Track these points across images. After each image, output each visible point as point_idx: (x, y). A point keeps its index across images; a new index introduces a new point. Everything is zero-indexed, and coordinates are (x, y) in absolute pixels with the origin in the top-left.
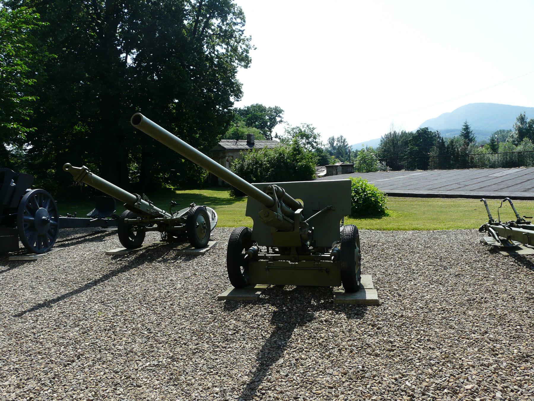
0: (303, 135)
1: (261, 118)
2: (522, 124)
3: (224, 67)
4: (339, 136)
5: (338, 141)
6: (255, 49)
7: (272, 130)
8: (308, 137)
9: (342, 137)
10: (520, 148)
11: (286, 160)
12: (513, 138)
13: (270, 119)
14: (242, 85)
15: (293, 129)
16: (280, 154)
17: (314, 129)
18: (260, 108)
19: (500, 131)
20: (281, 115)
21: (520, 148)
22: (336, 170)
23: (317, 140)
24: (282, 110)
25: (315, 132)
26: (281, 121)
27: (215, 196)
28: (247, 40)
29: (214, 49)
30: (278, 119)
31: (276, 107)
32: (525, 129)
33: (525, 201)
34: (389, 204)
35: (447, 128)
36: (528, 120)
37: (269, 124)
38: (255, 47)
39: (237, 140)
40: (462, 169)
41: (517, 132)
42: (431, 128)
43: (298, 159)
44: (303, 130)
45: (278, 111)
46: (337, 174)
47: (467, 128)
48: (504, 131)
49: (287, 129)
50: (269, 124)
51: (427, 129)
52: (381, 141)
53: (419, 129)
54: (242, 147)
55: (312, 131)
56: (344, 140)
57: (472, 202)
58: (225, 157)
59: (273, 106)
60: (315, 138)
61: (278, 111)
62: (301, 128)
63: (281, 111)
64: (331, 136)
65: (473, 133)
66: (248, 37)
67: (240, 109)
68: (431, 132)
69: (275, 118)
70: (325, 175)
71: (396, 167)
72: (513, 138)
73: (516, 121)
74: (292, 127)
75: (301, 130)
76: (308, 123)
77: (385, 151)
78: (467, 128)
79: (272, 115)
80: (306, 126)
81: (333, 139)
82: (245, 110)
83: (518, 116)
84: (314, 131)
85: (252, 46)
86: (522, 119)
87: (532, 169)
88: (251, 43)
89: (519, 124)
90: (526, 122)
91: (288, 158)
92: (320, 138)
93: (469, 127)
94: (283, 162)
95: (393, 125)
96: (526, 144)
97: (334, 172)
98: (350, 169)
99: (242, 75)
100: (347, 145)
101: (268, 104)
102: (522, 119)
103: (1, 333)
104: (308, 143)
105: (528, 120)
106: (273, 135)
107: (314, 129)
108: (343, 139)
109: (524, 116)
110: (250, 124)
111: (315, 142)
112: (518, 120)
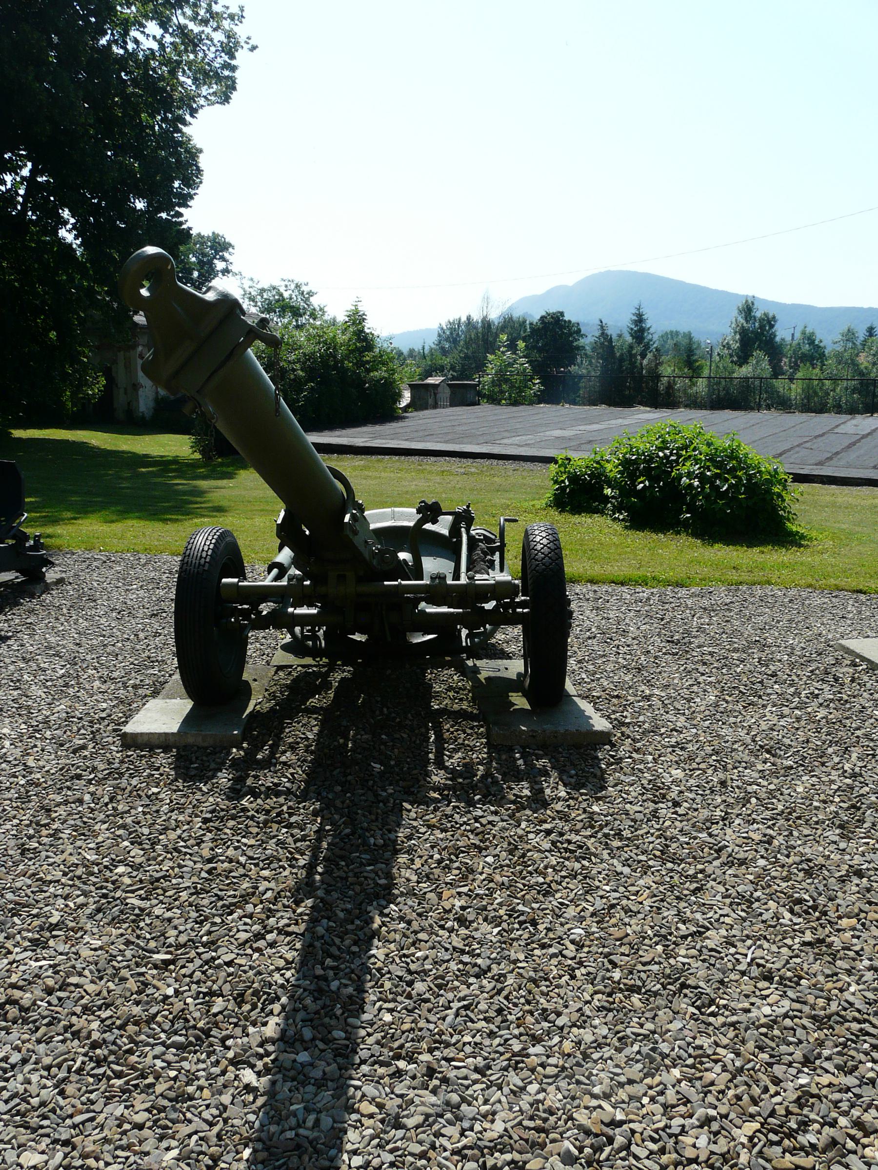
2: (747, 322)
6: (254, 48)
8: (296, 312)
10: (745, 371)
11: (342, 362)
12: (729, 348)
13: (201, 263)
14: (201, 151)
15: (263, 290)
17: (311, 294)
19: (672, 332)
20: (226, 255)
21: (745, 371)
22: (435, 394)
24: (230, 245)
25: (315, 301)
26: (226, 271)
27: (124, 448)
28: (232, 17)
29: (126, 33)
30: (220, 265)
31: (215, 236)
32: (752, 332)
34: (804, 507)
35: (597, 316)
37: (196, 274)
41: (738, 337)
42: (765, 302)
43: (368, 362)
44: (286, 295)
46: (435, 406)
47: (639, 319)
48: (677, 333)
49: (248, 290)
51: (562, 314)
52: (439, 335)
53: (544, 314)
55: (306, 301)
58: (134, 347)
62: (282, 289)
65: (651, 331)
66: (234, 10)
68: (570, 321)
69: (211, 263)
72: (729, 348)
73: (735, 313)
74: (260, 286)
75: (281, 295)
77: (467, 357)
78: (639, 319)
79: (204, 255)
80: (293, 286)
83: (740, 304)
84: (311, 299)
85: (242, 40)
88: (241, 31)
91: (346, 357)
93: (645, 317)
94: (335, 367)
95: (487, 300)
96: (757, 362)
97: (431, 401)
98: (470, 396)
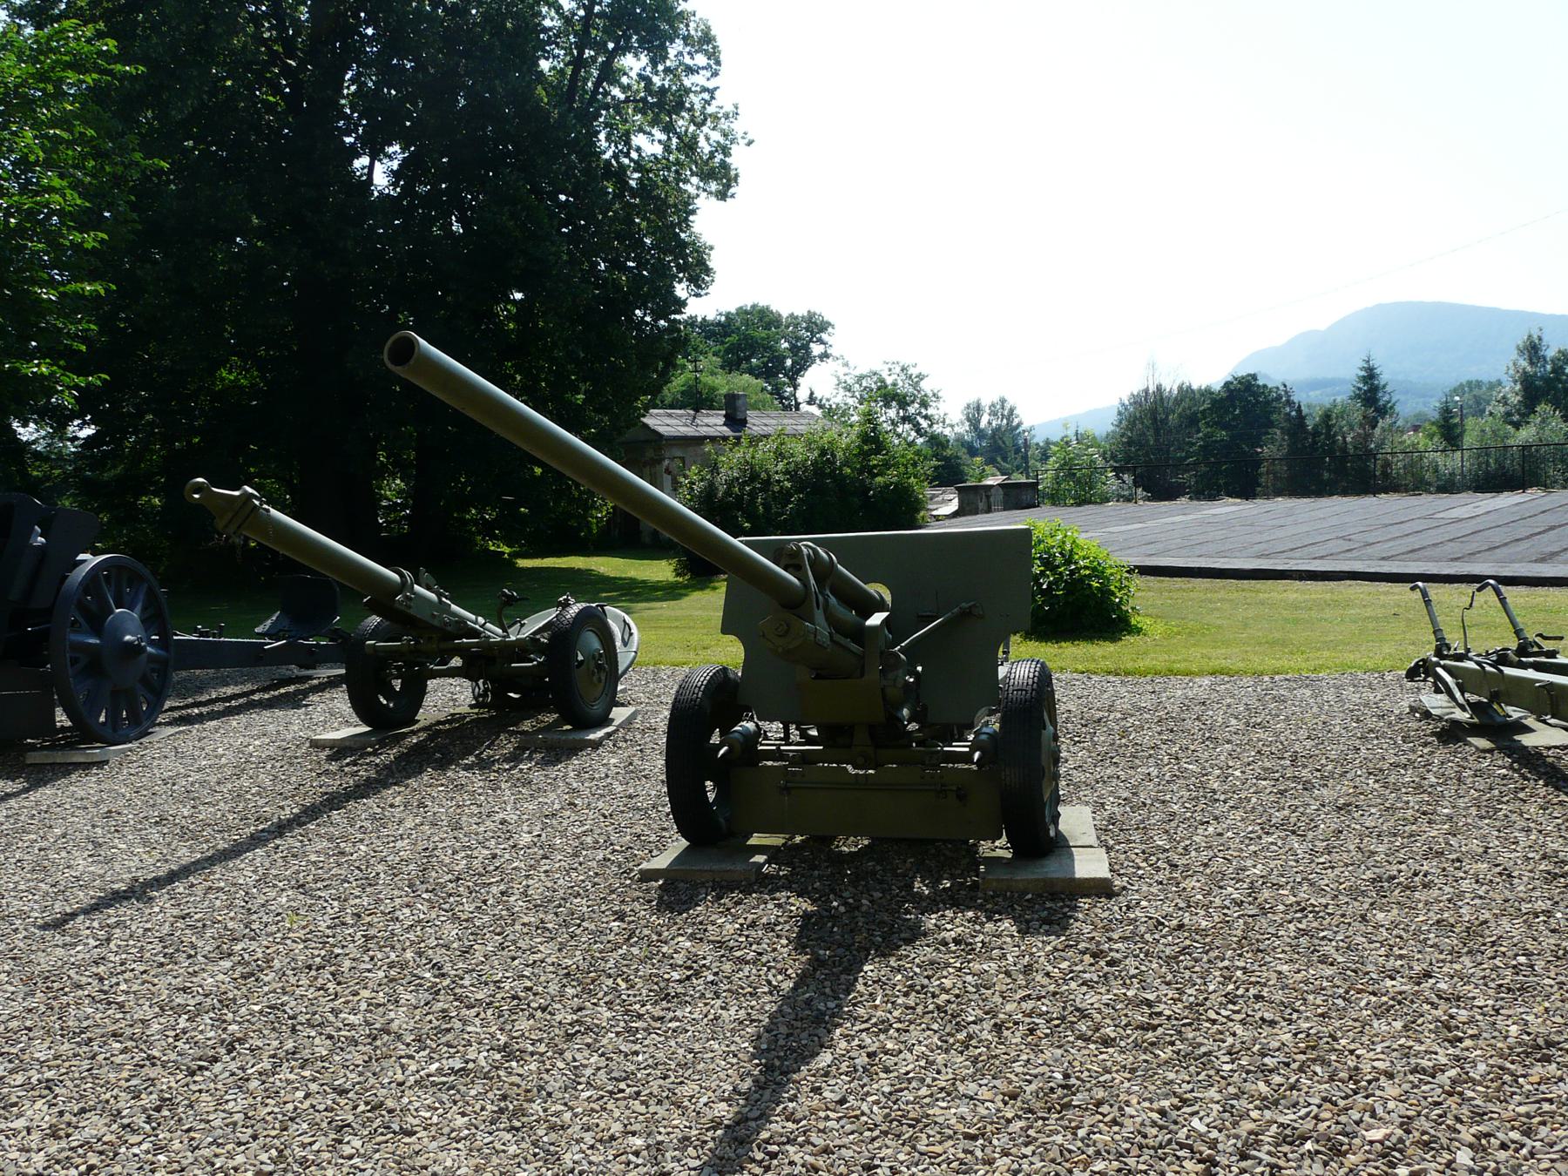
0: (890, 396)
1: (767, 347)
2: (1532, 363)
3: (658, 197)
4: (996, 399)
5: (993, 413)
6: (750, 143)
7: (800, 380)
8: (903, 402)
9: (1003, 401)
10: (1526, 434)
11: (840, 468)
12: (1506, 404)
13: (794, 349)
14: (711, 248)
15: (860, 378)
16: (823, 452)
17: (921, 377)
18: (763, 318)
19: (1469, 383)
20: (824, 336)
21: (1526, 434)
22: (988, 497)
23: (930, 411)
24: (829, 324)
25: (926, 386)
26: (825, 356)
27: (632, 574)
28: (727, 116)
29: (628, 143)
30: (816, 349)
31: (811, 315)
32: (1542, 378)
33: (1540, 590)
34: (1142, 598)
35: (1313, 376)
36: (1551, 353)
37: (789, 362)
38: (749, 137)
39: (697, 410)
40: (1358, 494)
41: (1518, 387)
42: (1266, 376)
43: (875, 466)
44: (889, 381)
45: (816, 326)
46: (989, 511)
47: (1370, 375)
48: (1479, 384)
49: (843, 378)
50: (789, 362)
51: (1254, 377)
52: (1120, 413)
53: (1230, 379)
54: (711, 432)
55: (915, 385)
56: (1012, 411)
57: (1386, 593)
58: (660, 461)
59: (801, 312)
60: (924, 404)
61: (816, 326)
62: (885, 375)
63: (824, 326)
64: (972, 399)
65: (1388, 389)
66: (729, 108)
67: (704, 319)
68: (1265, 386)
69: (806, 347)
70: (955, 515)
71: (1162, 491)
72: (1506, 404)
73: (1514, 355)
74: (857, 373)
75: (883, 381)
76: (905, 361)
77: (1130, 443)
78: (1370, 375)
79: (798, 339)
80: (898, 370)
81: (978, 408)
82: (719, 324)
83: (1521, 339)
84: (922, 384)
85: (739, 136)
86: (1533, 350)
87: (1561, 496)
88: (738, 127)
89: (1524, 363)
90: (1544, 357)
91: (846, 463)
92: (941, 405)
93: (1377, 371)
94: (832, 475)
95: (1153, 366)
96: (1543, 421)
97: (981, 505)
98: (1026, 497)
99: (710, 221)
100: (1019, 425)
101: (787, 304)
102: (1533, 350)
103: (3, 977)
104: (905, 419)
105: (1551, 353)
106: (802, 395)
107: (921, 377)
108: (1007, 406)
109: (1540, 339)
110: (733, 363)
111: (926, 417)
112: (1521, 352)
